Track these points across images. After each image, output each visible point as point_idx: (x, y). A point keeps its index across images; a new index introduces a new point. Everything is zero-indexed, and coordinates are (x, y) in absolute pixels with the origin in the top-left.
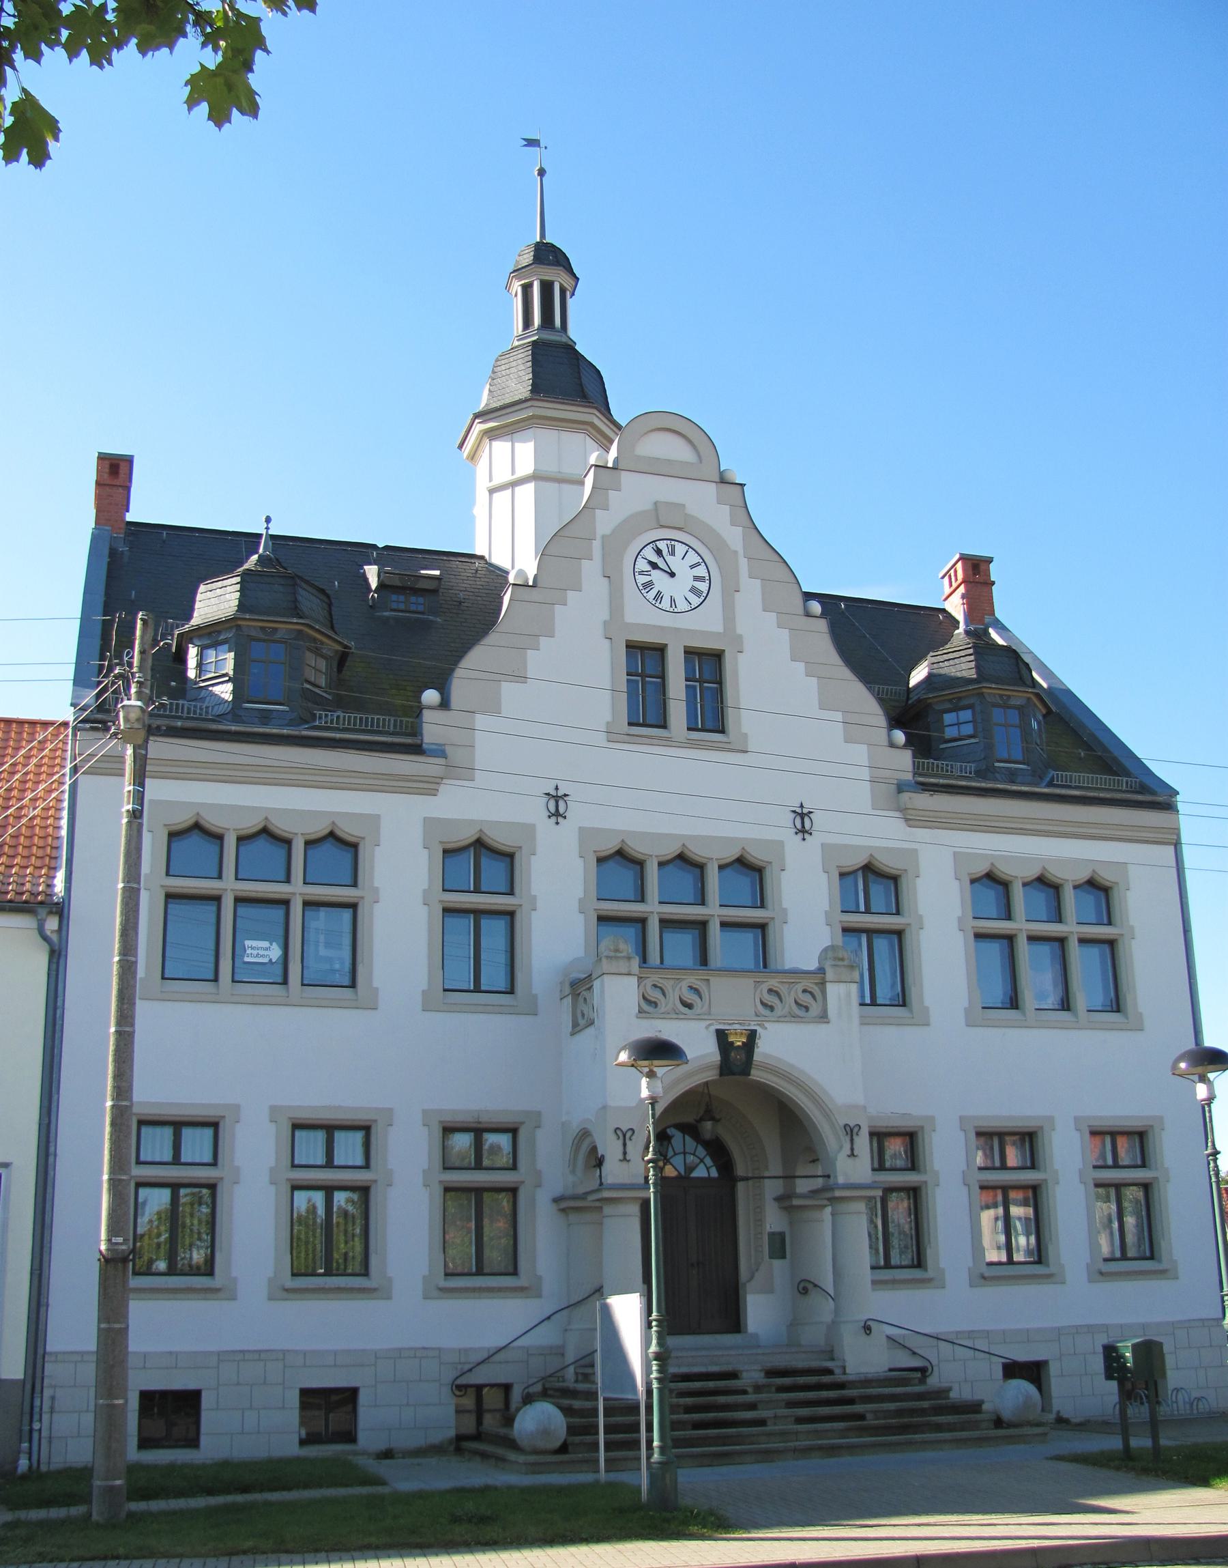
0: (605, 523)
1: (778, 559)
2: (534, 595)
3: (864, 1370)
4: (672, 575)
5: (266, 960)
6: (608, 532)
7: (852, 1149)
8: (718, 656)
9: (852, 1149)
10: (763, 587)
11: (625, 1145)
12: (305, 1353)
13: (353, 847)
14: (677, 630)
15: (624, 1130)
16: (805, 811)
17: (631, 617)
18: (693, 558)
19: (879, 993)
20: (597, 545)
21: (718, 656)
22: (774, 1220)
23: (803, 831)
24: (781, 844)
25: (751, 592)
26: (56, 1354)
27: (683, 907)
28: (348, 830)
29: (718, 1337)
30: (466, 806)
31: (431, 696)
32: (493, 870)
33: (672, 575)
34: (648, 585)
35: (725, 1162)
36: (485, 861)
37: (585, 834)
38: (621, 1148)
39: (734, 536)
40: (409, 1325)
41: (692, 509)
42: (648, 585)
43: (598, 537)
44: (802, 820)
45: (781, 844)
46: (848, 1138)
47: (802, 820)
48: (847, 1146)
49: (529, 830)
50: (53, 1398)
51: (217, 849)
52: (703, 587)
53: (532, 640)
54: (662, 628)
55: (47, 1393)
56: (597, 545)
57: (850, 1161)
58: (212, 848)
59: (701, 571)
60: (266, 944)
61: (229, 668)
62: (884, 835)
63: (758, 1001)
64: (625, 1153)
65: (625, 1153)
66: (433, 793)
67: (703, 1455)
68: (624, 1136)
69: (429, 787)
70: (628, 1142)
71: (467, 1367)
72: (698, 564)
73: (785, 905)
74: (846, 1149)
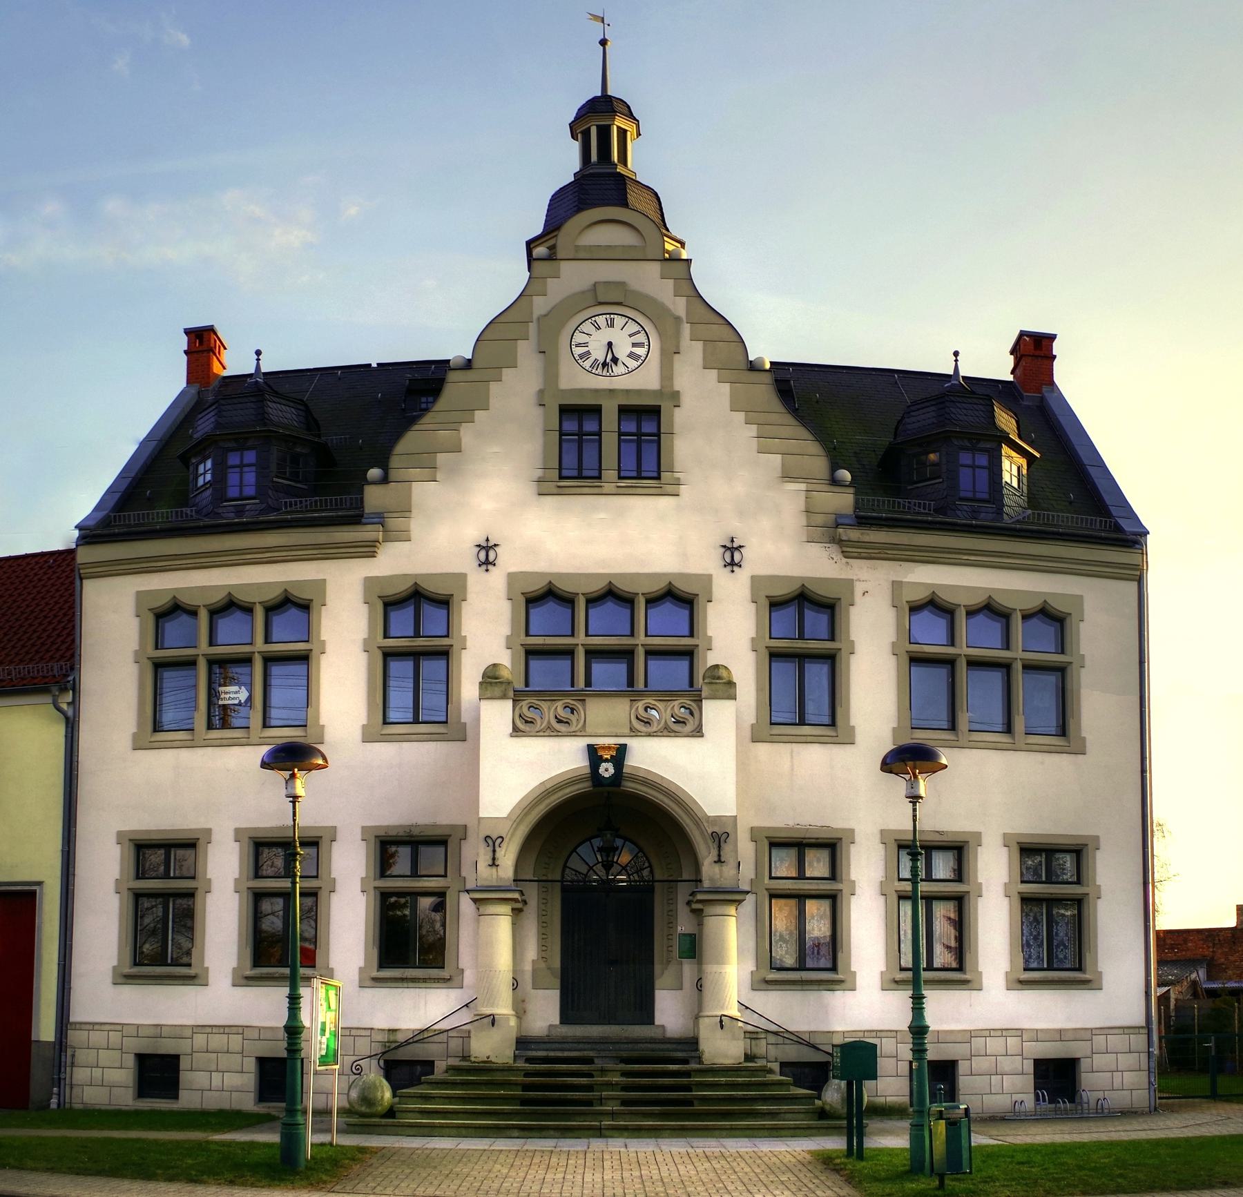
0: (540, 305)
1: (722, 321)
2: (470, 375)
3: (717, 1061)
4: (610, 344)
5: (236, 702)
6: (543, 312)
7: (719, 856)
8: (654, 412)
9: (719, 856)
10: (704, 346)
11: (494, 851)
12: (260, 1028)
13: (305, 607)
14: (611, 391)
15: (494, 837)
16: (491, 544)
17: (564, 384)
18: (633, 327)
19: (810, 708)
20: (532, 328)
21: (654, 412)
22: (684, 925)
23: (732, 564)
24: (709, 578)
25: (693, 352)
26: (76, 1023)
27: (612, 642)
28: (1059, 606)
29: (625, 1027)
30: (396, 562)
31: (374, 473)
32: (815, 621)
33: (610, 344)
34: (632, 355)
35: (615, 869)
36: (809, 615)
37: (512, 578)
38: (491, 854)
39: (679, 306)
40: (348, 1005)
41: (635, 285)
42: (632, 355)
43: (535, 317)
44: (732, 554)
45: (709, 578)
46: (716, 846)
47: (732, 554)
48: (714, 852)
49: (461, 578)
50: (73, 1056)
51: (687, 612)
52: (641, 351)
53: (467, 414)
54: (596, 391)
55: (69, 1052)
56: (532, 328)
57: (717, 868)
58: (563, 612)
59: (641, 338)
60: (235, 688)
61: (253, 461)
62: (817, 564)
63: (633, 717)
64: (494, 859)
65: (494, 859)
66: (373, 555)
67: (459, 1127)
68: (493, 843)
69: (368, 550)
70: (497, 849)
71: (393, 1045)
72: (638, 332)
73: (710, 633)
74: (713, 856)
